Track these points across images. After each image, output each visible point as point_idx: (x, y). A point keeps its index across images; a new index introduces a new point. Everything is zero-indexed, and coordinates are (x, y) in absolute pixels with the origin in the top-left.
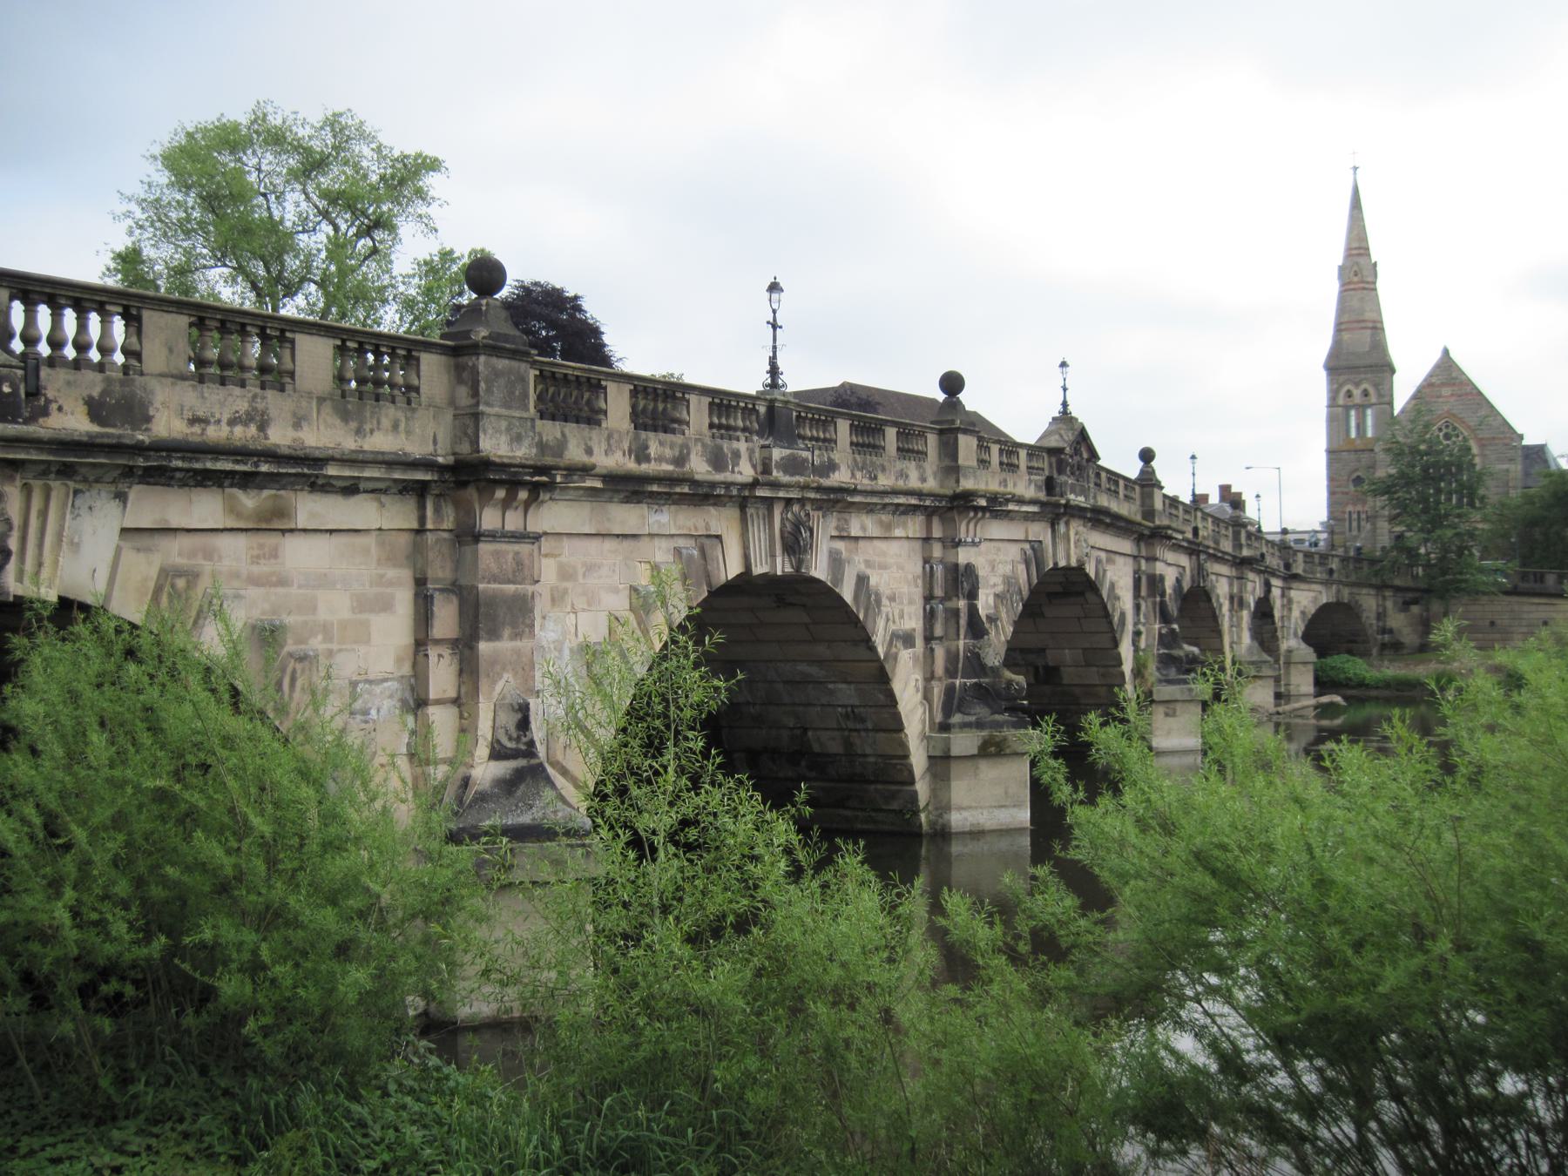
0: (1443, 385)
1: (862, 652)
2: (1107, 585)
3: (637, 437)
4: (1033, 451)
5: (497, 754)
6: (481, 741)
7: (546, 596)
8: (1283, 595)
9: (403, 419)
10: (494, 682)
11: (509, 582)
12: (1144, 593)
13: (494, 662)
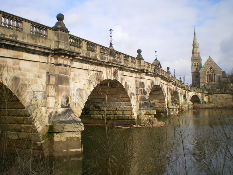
0: (210, 62)
1: (126, 96)
2: (163, 89)
3: (88, 52)
4: (152, 65)
5: (63, 107)
6: (59, 104)
7: (71, 78)
8: (187, 94)
9: (44, 41)
10: (62, 93)
11: (65, 74)
12: (168, 91)
13: (62, 89)
